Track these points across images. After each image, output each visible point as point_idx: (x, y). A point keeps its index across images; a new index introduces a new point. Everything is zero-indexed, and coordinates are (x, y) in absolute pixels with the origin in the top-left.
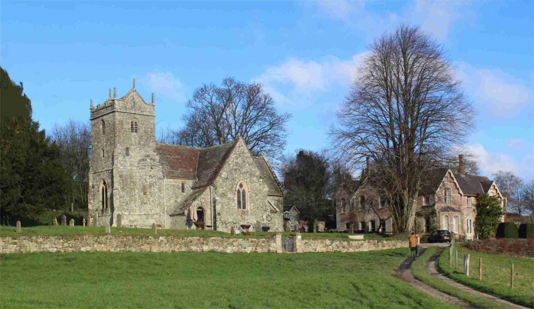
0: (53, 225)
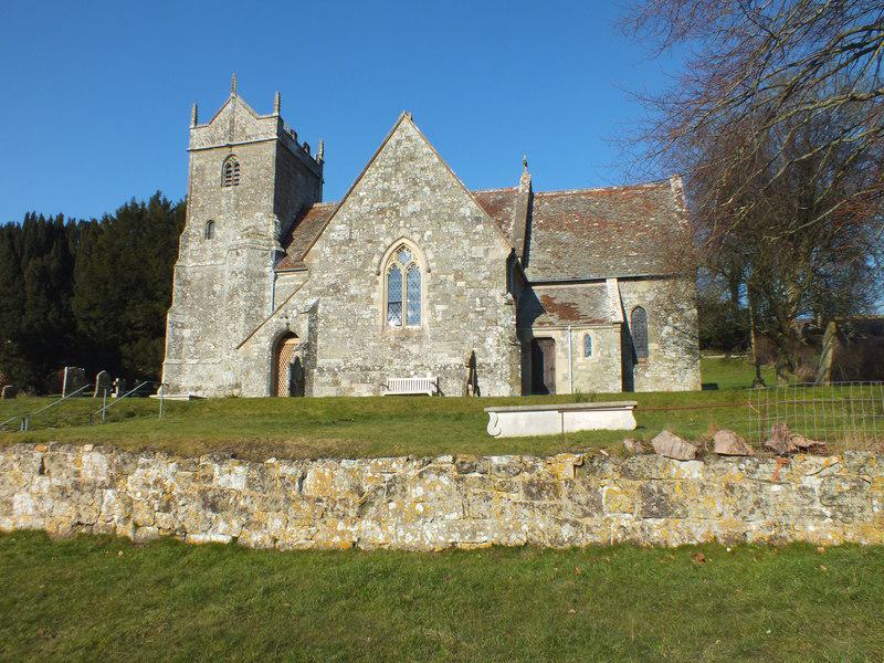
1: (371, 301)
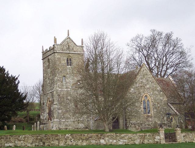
0: (4, 130)
1: (140, 108)
